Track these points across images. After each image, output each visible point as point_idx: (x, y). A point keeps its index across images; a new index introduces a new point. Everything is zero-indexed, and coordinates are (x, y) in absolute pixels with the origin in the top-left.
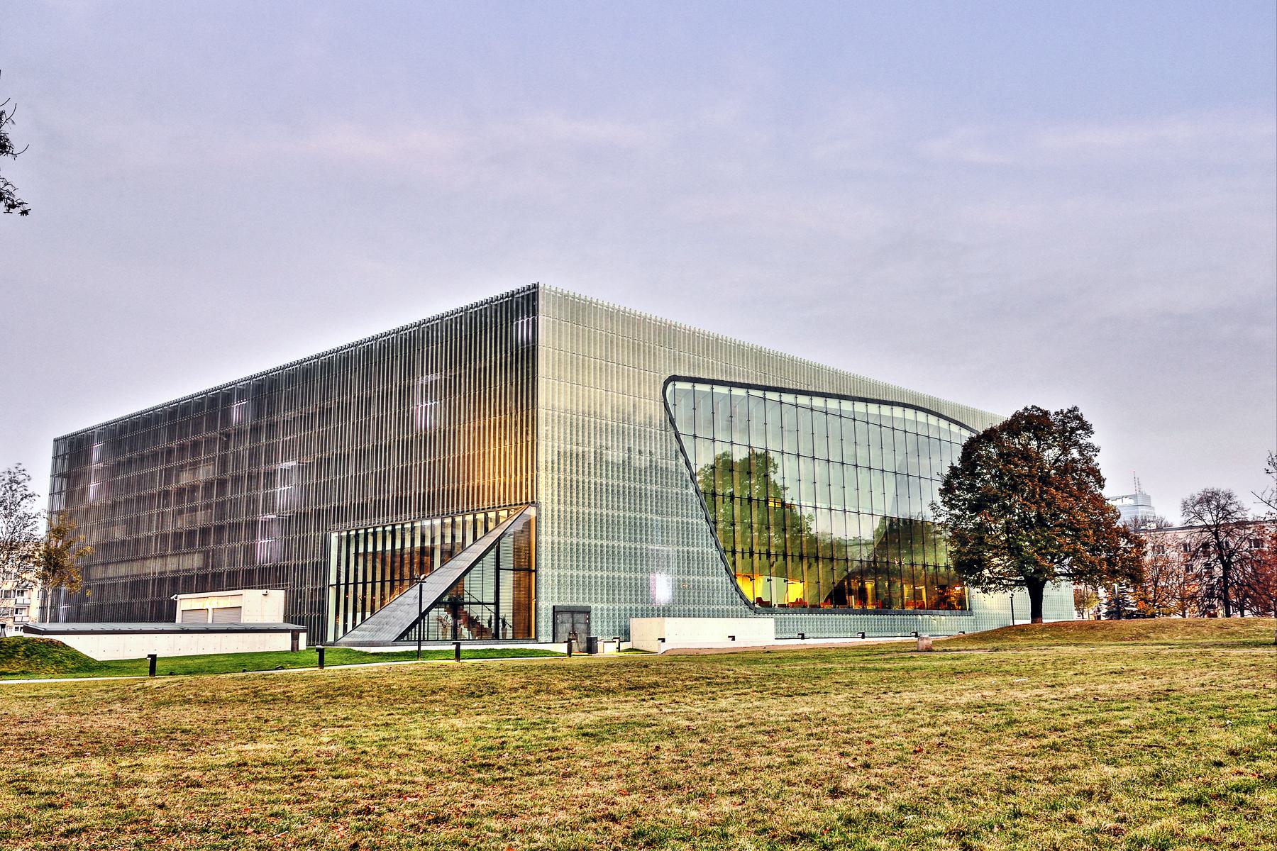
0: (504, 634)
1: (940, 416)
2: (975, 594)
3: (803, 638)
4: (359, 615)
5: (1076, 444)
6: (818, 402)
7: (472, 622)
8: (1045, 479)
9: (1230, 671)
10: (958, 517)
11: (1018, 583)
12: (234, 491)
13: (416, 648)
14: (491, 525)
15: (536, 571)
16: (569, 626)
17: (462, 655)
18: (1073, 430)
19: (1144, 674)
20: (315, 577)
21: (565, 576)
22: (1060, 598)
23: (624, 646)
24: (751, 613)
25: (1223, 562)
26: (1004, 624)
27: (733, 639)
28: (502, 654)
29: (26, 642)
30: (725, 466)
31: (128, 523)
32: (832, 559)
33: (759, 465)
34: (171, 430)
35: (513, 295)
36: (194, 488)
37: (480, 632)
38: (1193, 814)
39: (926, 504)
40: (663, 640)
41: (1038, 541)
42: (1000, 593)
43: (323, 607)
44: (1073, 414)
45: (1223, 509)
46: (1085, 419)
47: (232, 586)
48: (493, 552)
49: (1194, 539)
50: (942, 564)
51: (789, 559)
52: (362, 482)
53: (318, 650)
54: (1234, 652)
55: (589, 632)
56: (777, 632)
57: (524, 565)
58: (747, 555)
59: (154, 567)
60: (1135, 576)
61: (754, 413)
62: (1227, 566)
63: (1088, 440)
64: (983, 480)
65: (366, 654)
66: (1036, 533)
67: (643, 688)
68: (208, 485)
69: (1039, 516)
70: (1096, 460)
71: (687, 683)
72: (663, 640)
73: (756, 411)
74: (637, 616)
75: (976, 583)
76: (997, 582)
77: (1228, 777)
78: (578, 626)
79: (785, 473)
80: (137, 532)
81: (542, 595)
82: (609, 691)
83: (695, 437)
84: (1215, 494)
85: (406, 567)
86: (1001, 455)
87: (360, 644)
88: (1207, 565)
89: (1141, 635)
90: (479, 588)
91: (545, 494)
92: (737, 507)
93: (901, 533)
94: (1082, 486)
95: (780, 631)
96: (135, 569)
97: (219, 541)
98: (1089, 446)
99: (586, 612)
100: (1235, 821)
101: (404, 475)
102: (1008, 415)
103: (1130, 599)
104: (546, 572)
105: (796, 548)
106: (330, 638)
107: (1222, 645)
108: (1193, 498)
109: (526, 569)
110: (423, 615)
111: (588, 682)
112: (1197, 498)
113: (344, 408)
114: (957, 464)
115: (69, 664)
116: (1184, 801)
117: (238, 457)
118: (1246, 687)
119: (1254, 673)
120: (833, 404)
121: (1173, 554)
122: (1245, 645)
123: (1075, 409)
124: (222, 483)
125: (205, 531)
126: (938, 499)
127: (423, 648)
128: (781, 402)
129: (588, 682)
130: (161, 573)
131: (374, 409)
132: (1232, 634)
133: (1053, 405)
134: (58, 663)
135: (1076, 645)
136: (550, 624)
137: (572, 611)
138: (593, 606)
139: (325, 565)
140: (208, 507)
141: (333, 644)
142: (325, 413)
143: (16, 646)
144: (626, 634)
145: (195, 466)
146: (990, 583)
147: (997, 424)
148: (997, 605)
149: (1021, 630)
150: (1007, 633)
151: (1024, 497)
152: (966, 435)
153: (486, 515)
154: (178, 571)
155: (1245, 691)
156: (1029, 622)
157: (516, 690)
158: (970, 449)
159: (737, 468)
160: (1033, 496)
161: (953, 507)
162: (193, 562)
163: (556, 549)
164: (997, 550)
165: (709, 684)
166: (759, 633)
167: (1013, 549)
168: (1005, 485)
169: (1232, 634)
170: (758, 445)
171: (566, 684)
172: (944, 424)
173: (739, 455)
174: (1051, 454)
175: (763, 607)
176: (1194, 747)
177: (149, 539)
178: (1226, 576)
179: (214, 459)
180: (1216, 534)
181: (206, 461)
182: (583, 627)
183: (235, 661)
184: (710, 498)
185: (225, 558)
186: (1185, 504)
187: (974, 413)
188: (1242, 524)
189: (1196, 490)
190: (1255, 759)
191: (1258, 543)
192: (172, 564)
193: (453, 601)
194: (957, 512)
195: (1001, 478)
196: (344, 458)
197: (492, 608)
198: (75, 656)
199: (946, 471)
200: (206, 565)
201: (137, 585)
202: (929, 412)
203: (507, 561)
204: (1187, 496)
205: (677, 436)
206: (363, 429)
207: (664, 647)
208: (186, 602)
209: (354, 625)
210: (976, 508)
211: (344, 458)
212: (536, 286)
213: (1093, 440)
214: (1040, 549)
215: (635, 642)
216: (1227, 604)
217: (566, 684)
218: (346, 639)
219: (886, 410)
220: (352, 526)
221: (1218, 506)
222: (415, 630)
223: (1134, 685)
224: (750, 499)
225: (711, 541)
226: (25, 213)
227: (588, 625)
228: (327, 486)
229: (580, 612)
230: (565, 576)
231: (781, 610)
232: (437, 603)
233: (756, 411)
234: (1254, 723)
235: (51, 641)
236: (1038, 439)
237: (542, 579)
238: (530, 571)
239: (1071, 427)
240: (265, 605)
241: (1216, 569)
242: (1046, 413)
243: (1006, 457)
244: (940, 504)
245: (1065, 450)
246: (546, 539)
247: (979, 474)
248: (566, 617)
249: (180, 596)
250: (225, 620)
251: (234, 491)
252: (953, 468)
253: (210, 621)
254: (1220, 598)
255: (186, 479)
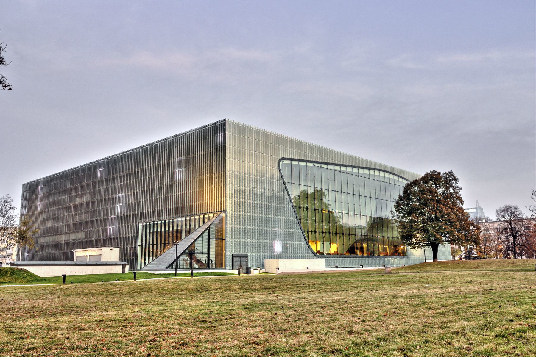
0: (212, 266)
1: (394, 174)
2: (409, 249)
3: (337, 267)
4: (151, 258)
5: (452, 186)
6: (343, 169)
7: (198, 261)
8: (439, 201)
9: (516, 282)
10: (402, 217)
11: (427, 245)
12: (99, 206)
13: (175, 272)
14: (206, 220)
15: (225, 240)
16: (239, 262)
17: (194, 275)
18: (450, 180)
19: (480, 283)
20: (132, 242)
21: (237, 241)
22: (445, 250)
23: (262, 271)
24: (315, 257)
25: (513, 236)
26: (421, 262)
27: (308, 268)
28: (211, 274)
29: (11, 269)
30: (304, 196)
31: (54, 219)
32: (349, 235)
33: (319, 195)
34: (72, 180)
35: (215, 124)
36: (81, 205)
37: (202, 265)
38: (501, 341)
39: (389, 211)
40: (278, 269)
41: (435, 227)
42: (419, 249)
43: (135, 255)
44: (450, 174)
45: (513, 213)
46: (455, 176)
47: (97, 246)
48: (207, 232)
49: (501, 226)
50: (395, 237)
51: (331, 234)
52: (152, 202)
53: (133, 273)
54: (518, 273)
55: (247, 265)
56: (326, 265)
57: (220, 237)
58: (314, 233)
59: (64, 238)
60: (476, 242)
61: (316, 173)
62: (515, 237)
63: (457, 184)
64: (413, 201)
65: (154, 274)
66: (435, 224)
67: (270, 288)
68: (87, 204)
69: (436, 217)
70: (460, 193)
71: (289, 286)
72: (278, 269)
73: (317, 172)
74: (267, 258)
75: (410, 245)
76: (419, 244)
77: (516, 326)
78: (242, 262)
79: (329, 198)
80: (58, 223)
81: (228, 250)
82: (256, 290)
83: (292, 183)
84: (510, 207)
85: (169, 238)
86: (420, 191)
87: (151, 270)
88: (507, 237)
89: (479, 266)
90: (201, 247)
91: (229, 208)
92: (309, 213)
93: (378, 224)
94: (454, 204)
95: (327, 265)
96: (57, 238)
97: (92, 227)
98: (457, 187)
99: (246, 257)
100: (519, 344)
101: (169, 199)
102: (423, 174)
103: (474, 251)
104: (229, 240)
105: (334, 230)
106: (139, 268)
107: (513, 271)
108: (501, 209)
109: (221, 239)
110: (178, 258)
111: (247, 286)
112: (503, 209)
113: (144, 171)
114: (402, 195)
115: (29, 278)
116: (497, 336)
117: (100, 192)
118: (523, 288)
119: (526, 282)
120: (349, 170)
121: (492, 232)
122: (522, 270)
123: (451, 172)
124: (93, 203)
125: (86, 223)
126: (394, 209)
127: (177, 272)
128: (328, 169)
129: (247, 286)
130: (68, 240)
131: (157, 171)
132: (517, 266)
133: (442, 170)
134: (24, 278)
135: (452, 271)
136: (231, 262)
137: (240, 256)
138: (249, 254)
139: (137, 237)
140: (87, 213)
141: (140, 270)
142: (136, 173)
143: (7, 271)
144: (263, 266)
145: (82, 196)
146: (416, 244)
147: (418, 178)
148: (418, 253)
149: (429, 264)
150: (422, 265)
151: (429, 209)
152: (406, 182)
153: (204, 216)
154: (75, 240)
155: (522, 290)
156: (432, 261)
157: (216, 289)
158: (407, 189)
159: (309, 196)
160: (434, 208)
161: (400, 213)
162: (81, 236)
163: (233, 230)
164: (418, 231)
165: (297, 287)
166: (319, 265)
167: (425, 230)
168: (422, 204)
169: (517, 266)
170: (318, 187)
171: (237, 287)
172: (396, 178)
173: (310, 191)
174: (441, 190)
175: (320, 255)
176: (501, 313)
177: (62, 226)
178: (514, 242)
179: (90, 193)
180: (510, 224)
181: (86, 193)
182: (245, 263)
183: (99, 277)
184: (298, 209)
185: (95, 234)
186: (497, 212)
187: (409, 173)
188: (521, 220)
189: (502, 205)
190: (526, 318)
191: (528, 228)
192: (72, 237)
193: (190, 253)
194: (402, 215)
195: (420, 200)
196: (144, 192)
197: (207, 255)
198: (31, 275)
199: (397, 198)
200: (86, 237)
201: (57, 245)
202: (390, 173)
203: (213, 236)
204: (498, 208)
205: (284, 183)
206: (152, 180)
207: (279, 272)
208: (78, 253)
209: (149, 262)
210: (410, 213)
211: (144, 192)
212: (225, 120)
213: (459, 184)
214: (437, 230)
215: (267, 269)
216: (515, 253)
217: (237, 287)
218: (145, 268)
219: (372, 172)
220: (148, 221)
221: (511, 213)
222: (174, 264)
223: (476, 287)
224: (315, 209)
225: (298, 227)
226: (10, 89)
227: (247, 262)
228: (137, 204)
229: (243, 257)
230: (237, 241)
231: (328, 256)
232: (183, 253)
233: (317, 172)
234: (527, 303)
235: (21, 269)
236: (436, 184)
237: (228, 243)
238: (222, 239)
239: (449, 179)
240: (111, 254)
241: (511, 239)
242: (439, 173)
243: (422, 192)
244: (395, 212)
245: (447, 189)
246: (229, 226)
247: (411, 199)
248: (238, 259)
249: (76, 250)
250: (94, 261)
251: (99, 206)
252: (400, 196)
253: (88, 260)
254: (512, 251)
255: (78, 201)
